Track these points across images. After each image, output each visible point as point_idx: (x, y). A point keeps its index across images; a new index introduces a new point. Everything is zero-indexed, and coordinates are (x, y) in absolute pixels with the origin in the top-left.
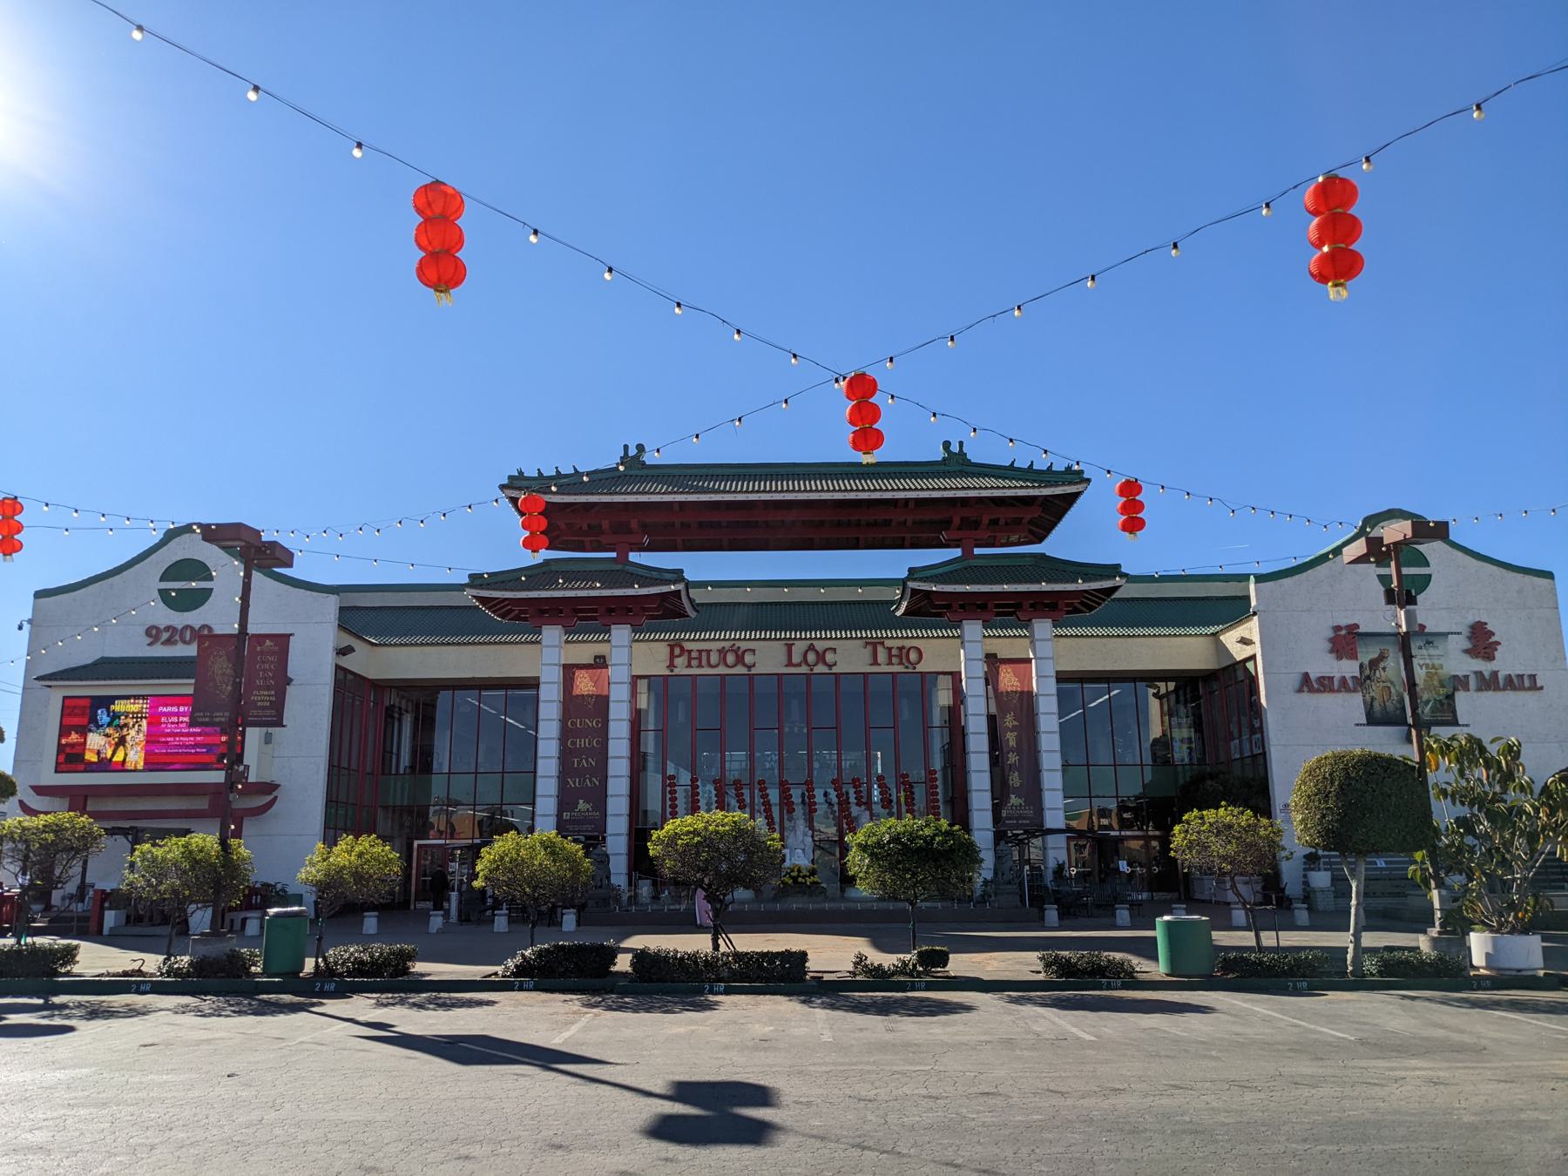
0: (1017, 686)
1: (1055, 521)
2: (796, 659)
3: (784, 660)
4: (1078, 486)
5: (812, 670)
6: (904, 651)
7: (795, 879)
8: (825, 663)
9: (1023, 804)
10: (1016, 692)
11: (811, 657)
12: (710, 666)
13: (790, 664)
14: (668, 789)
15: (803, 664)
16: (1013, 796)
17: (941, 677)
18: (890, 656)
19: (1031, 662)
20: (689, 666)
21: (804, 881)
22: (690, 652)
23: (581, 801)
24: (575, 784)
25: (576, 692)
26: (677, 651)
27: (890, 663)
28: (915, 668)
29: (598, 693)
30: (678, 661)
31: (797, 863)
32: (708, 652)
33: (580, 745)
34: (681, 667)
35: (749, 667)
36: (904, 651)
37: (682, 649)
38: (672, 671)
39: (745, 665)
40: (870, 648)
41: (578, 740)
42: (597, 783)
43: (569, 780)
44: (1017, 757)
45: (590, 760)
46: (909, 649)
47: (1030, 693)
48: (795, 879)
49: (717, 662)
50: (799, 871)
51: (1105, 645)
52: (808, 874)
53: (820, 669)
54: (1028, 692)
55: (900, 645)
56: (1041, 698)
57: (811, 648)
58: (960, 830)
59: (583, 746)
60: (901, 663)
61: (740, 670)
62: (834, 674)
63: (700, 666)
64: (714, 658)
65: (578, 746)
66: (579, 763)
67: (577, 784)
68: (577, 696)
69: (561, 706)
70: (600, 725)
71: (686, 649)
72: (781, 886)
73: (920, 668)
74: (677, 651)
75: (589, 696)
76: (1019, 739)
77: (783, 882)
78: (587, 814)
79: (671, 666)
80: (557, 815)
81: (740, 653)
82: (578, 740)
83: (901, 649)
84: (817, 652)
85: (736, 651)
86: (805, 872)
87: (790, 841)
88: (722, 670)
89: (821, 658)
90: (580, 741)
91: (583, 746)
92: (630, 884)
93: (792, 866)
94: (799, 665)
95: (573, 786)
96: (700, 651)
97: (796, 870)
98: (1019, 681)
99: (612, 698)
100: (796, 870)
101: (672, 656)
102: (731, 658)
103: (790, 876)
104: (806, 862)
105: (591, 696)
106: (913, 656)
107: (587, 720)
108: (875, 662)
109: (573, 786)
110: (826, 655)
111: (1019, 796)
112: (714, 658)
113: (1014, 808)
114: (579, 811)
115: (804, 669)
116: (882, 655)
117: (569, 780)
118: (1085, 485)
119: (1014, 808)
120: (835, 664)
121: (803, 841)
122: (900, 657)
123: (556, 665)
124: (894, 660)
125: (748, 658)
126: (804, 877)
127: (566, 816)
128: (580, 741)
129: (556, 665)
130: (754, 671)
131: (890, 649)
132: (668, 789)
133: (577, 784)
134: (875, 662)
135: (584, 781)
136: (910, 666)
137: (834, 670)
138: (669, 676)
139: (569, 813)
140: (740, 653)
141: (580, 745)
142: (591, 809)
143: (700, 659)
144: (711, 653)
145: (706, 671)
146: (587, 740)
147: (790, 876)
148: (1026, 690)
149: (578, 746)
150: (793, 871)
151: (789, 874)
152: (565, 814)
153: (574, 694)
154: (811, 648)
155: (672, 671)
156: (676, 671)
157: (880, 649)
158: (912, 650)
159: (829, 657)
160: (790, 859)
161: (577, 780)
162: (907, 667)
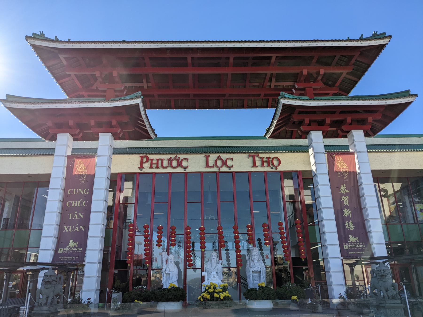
0: (346, 169)
1: (356, 79)
2: (211, 164)
3: (204, 165)
4: (384, 40)
5: (219, 169)
6: (270, 160)
7: (211, 294)
8: (227, 166)
9: (358, 241)
10: (346, 172)
11: (219, 163)
12: (163, 167)
13: (207, 166)
14: (188, 263)
15: (214, 167)
16: (351, 236)
17: (292, 173)
18: (263, 162)
19: (354, 154)
20: (151, 167)
21: (218, 296)
22: (152, 160)
23: (71, 241)
24: (68, 229)
25: (75, 172)
26: (145, 160)
27: (263, 166)
28: (277, 169)
29: (88, 174)
30: (145, 165)
31: (213, 282)
32: (162, 160)
33: (75, 205)
34: (147, 169)
35: (185, 168)
36: (270, 160)
37: (148, 158)
38: (141, 170)
39: (182, 167)
40: (251, 158)
41: (73, 202)
42: (83, 229)
43: (65, 227)
44: (350, 212)
45: (80, 214)
46: (273, 158)
47: (355, 173)
48: (211, 294)
49: (167, 166)
50: (215, 288)
51: (379, 156)
52: (221, 290)
53: (224, 169)
54: (353, 172)
55: (268, 156)
56: (362, 176)
57: (219, 158)
58: (136, 278)
59: (76, 206)
60: (269, 166)
61: (180, 170)
62: (232, 172)
63: (157, 167)
64: (165, 164)
65: (73, 206)
66: (72, 216)
67: (70, 230)
68: (76, 175)
69: (64, 180)
70: (88, 192)
71: (150, 158)
72: (202, 300)
73: (280, 169)
74: (145, 160)
75: (82, 175)
76: (350, 200)
77: (202, 297)
78: (74, 249)
79: (141, 167)
80: (55, 250)
81: (180, 161)
82: (73, 202)
83: (268, 158)
84: (222, 160)
85: (177, 160)
86: (219, 289)
87: (206, 267)
88: (170, 170)
89: (224, 163)
90: (75, 203)
91: (76, 206)
92: (101, 300)
93: (209, 284)
94: (212, 167)
95: (67, 231)
96: (158, 160)
97: (212, 287)
98: (347, 165)
99: (96, 176)
100: (212, 287)
101: (142, 163)
102: (175, 164)
103: (208, 292)
104: (220, 282)
105: (84, 175)
106: (275, 162)
107: (80, 190)
108: (254, 165)
109: (67, 231)
110: (227, 162)
111: (355, 236)
112: (165, 164)
113: (353, 244)
114: (69, 247)
115: (215, 169)
116: (258, 162)
117: (65, 227)
118: (388, 40)
119: (353, 244)
120: (232, 166)
121: (216, 267)
122: (268, 162)
123: (63, 156)
124: (265, 164)
125: (184, 164)
126: (218, 293)
127: (60, 251)
128: (75, 203)
129: (63, 156)
130: (187, 170)
131: (262, 159)
132: (188, 263)
133: (70, 230)
134: (254, 165)
135: (75, 228)
136: (274, 168)
137: (232, 170)
138: (139, 173)
139: (62, 249)
140: (180, 161)
141: (75, 205)
142: (77, 246)
143: (157, 164)
144: (164, 161)
145: (161, 170)
146: (79, 202)
147: (208, 292)
148: (352, 171)
149: (73, 206)
150: (210, 288)
151: (207, 290)
152: (60, 249)
153: (73, 174)
154: (219, 158)
155: (141, 170)
156: (144, 171)
157: (257, 159)
158: (274, 160)
159: (229, 163)
160: (208, 280)
161: (70, 227)
162: (272, 168)
